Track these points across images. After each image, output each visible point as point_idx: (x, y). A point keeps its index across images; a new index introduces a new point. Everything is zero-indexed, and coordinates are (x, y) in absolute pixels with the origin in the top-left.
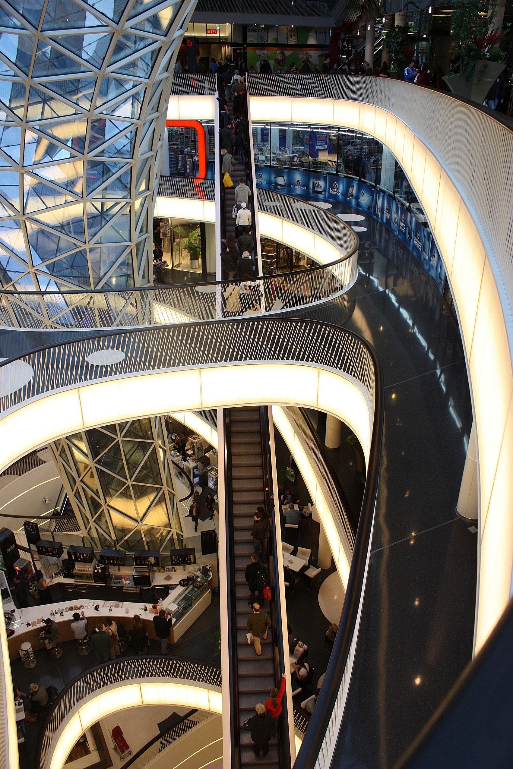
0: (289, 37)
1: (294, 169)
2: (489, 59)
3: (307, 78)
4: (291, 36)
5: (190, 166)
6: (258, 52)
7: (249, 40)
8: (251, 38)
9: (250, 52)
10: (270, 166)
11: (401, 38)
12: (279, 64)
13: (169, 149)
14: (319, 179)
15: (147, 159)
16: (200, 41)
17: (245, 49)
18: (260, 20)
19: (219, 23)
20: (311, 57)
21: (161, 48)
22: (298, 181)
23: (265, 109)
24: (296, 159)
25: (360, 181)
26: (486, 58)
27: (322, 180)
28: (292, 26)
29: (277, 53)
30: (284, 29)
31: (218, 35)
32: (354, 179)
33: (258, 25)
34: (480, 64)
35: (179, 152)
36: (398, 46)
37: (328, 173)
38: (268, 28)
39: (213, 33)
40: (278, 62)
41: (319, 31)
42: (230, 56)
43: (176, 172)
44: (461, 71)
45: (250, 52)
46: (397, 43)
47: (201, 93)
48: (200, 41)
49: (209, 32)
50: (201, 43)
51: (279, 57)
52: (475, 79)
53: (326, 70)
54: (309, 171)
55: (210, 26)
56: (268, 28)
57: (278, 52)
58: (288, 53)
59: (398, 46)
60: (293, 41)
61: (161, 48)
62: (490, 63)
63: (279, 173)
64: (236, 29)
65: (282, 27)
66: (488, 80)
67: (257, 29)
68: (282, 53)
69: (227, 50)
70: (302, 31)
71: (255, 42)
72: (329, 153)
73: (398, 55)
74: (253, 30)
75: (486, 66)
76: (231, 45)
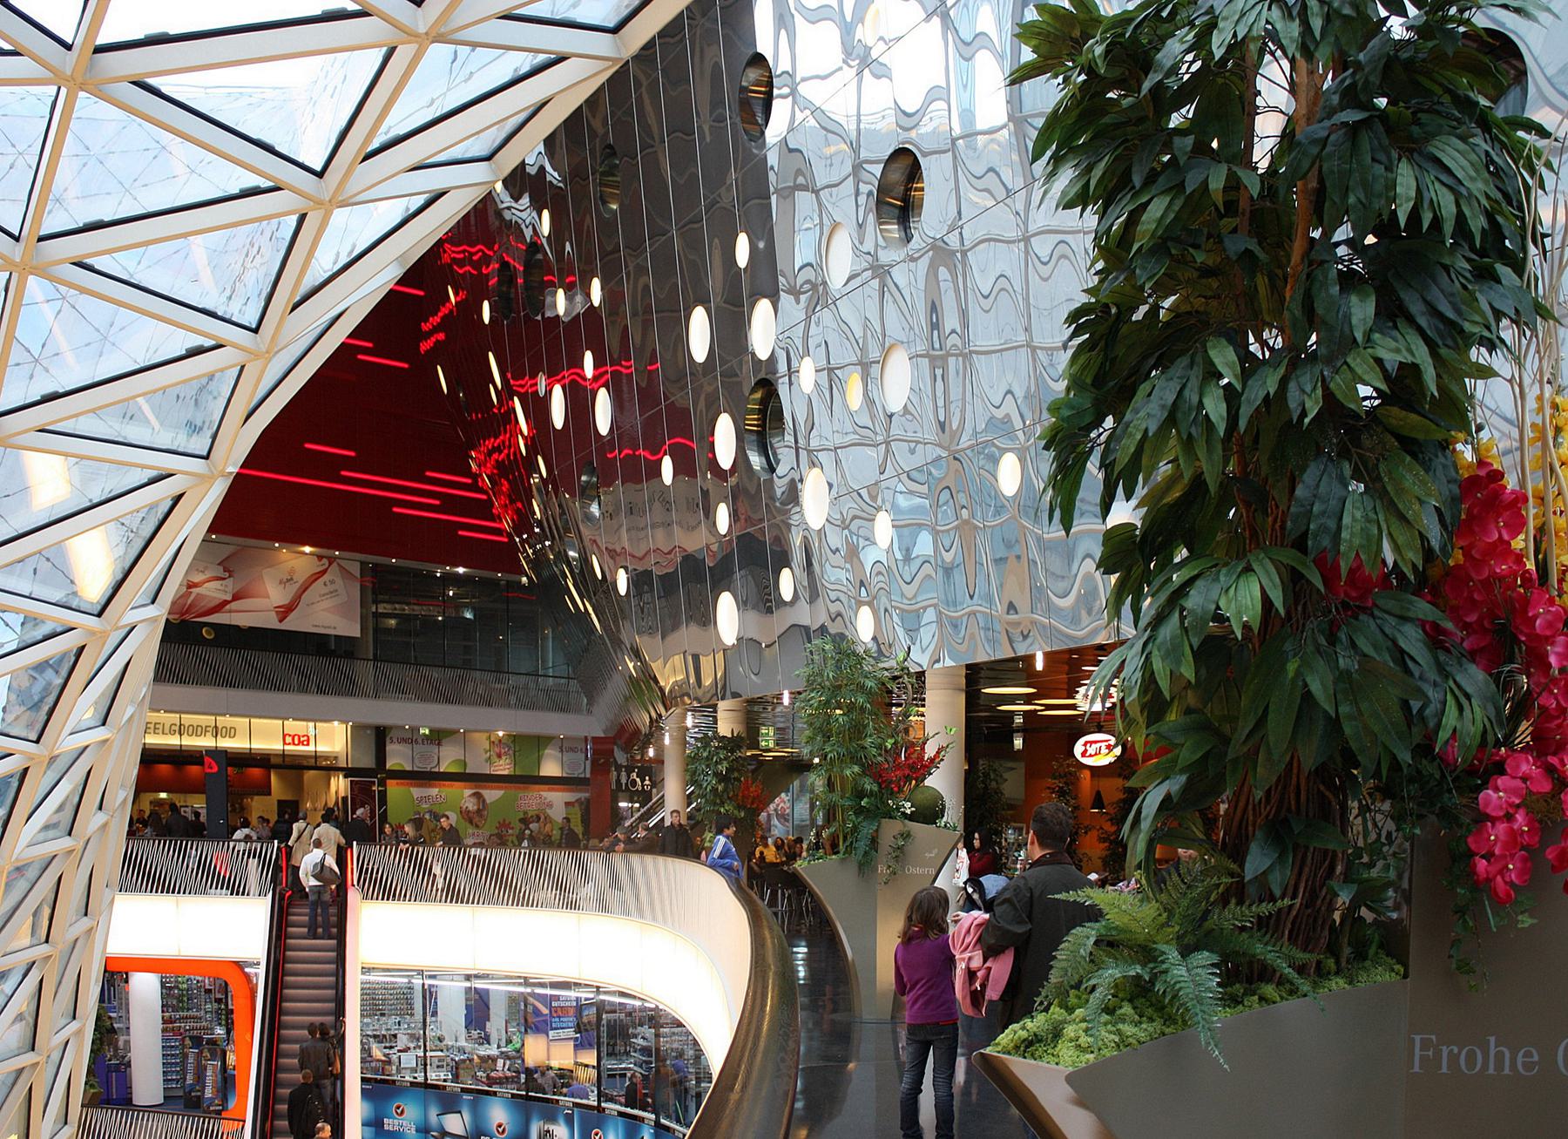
0: (494, 758)
1: (487, 1093)
2: (911, 817)
3: (514, 861)
4: (499, 756)
5: (215, 1082)
6: (416, 792)
7: (391, 764)
8: (397, 758)
9: (394, 790)
10: (426, 1085)
11: (725, 764)
12: (471, 822)
13: (164, 1030)
14: (552, 1119)
15: (20, 1071)
16: (273, 761)
17: (382, 783)
18: (419, 715)
19: (315, 721)
20: (550, 805)
21: (26, 770)
22: (500, 1126)
23: (393, 936)
24: (500, 1062)
25: (658, 1124)
26: (904, 813)
27: (561, 1121)
28: (501, 734)
29: (464, 795)
30: (481, 740)
31: (311, 748)
32: (642, 1120)
33: (414, 730)
34: (890, 830)
35: (188, 1042)
36: (719, 782)
37: (576, 1105)
38: (438, 737)
39: (301, 743)
40: (467, 816)
41: (566, 746)
42: (345, 799)
43: (181, 1093)
44: (842, 847)
45: (394, 790)
46: (716, 774)
47: (237, 888)
48: (273, 761)
49: (288, 740)
50: (276, 767)
51: (471, 805)
52: (882, 869)
53: (570, 841)
54: (528, 1098)
55: (294, 726)
56: (438, 737)
57: (468, 792)
58: (492, 795)
59: (719, 782)
60: (503, 767)
61: (26, 770)
62: (916, 827)
63: (449, 1104)
64: (358, 730)
65: (477, 735)
66: (919, 871)
67: (411, 738)
68: (478, 795)
69: (340, 785)
70: (528, 745)
71: (409, 768)
72: (186, 1107)
73: (722, 804)
74: (403, 741)
75: (906, 836)
76: (348, 772)
